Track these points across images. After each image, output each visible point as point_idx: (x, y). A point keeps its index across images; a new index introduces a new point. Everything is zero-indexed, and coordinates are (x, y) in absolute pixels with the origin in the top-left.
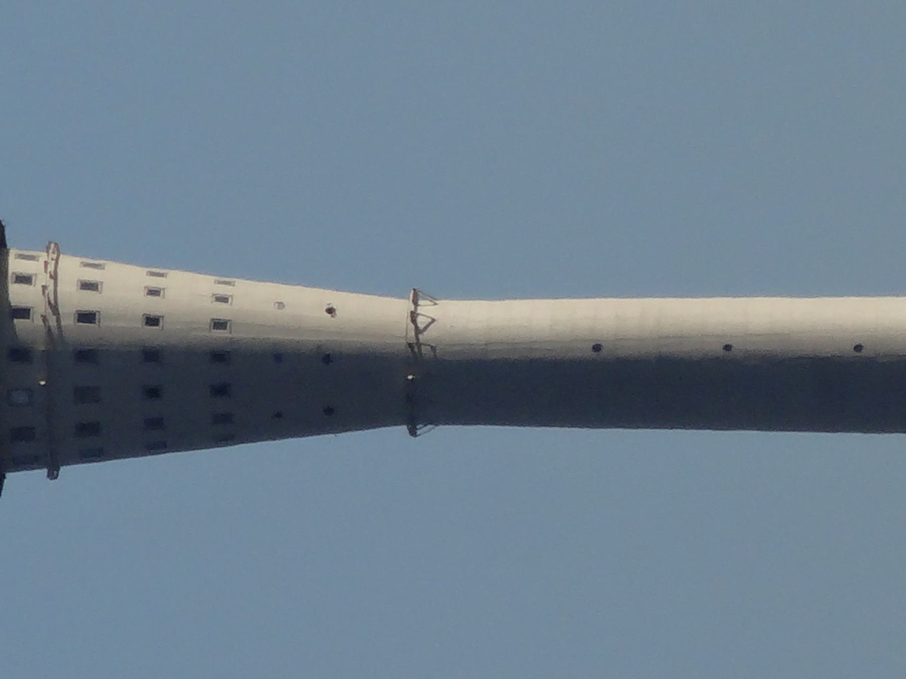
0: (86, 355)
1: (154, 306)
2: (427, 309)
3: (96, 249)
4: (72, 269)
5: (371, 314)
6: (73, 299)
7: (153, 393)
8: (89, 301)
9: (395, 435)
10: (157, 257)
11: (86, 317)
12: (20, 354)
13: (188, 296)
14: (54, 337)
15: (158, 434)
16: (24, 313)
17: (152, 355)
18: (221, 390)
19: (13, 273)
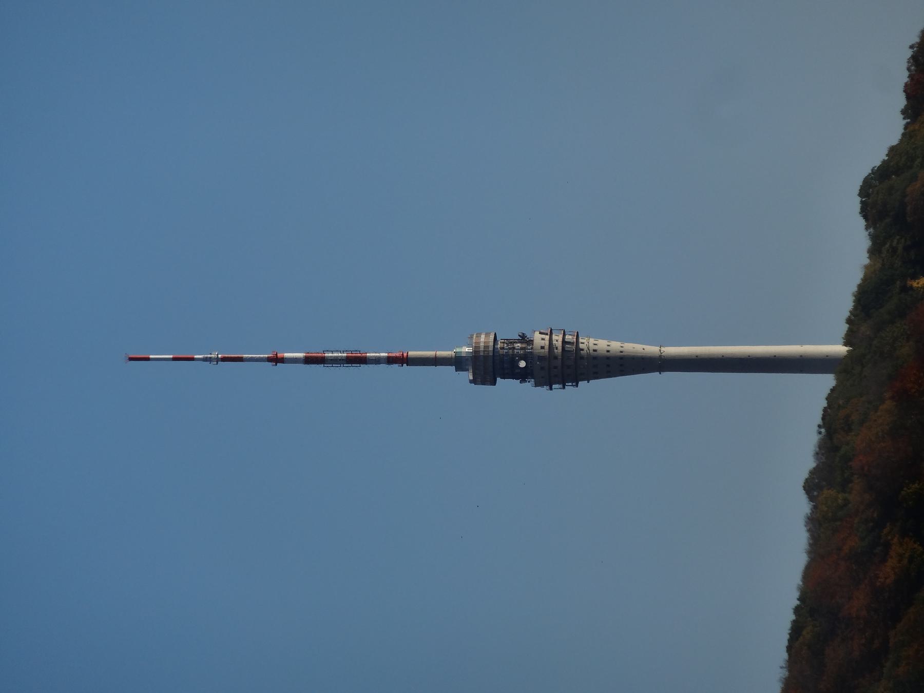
0: (595, 358)
1: (609, 348)
2: (663, 349)
3: (597, 337)
4: (592, 341)
5: (651, 350)
6: (592, 347)
7: (608, 366)
8: (596, 347)
9: (516, 382)
10: (610, 339)
11: (595, 351)
12: (582, 358)
13: (616, 346)
14: (589, 354)
15: (609, 374)
16: (583, 350)
17: (608, 358)
18: (621, 365)
19: (467, 370)
